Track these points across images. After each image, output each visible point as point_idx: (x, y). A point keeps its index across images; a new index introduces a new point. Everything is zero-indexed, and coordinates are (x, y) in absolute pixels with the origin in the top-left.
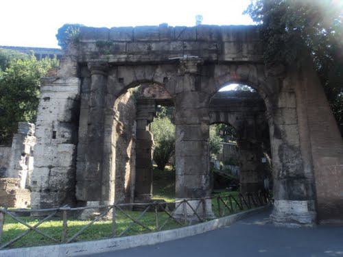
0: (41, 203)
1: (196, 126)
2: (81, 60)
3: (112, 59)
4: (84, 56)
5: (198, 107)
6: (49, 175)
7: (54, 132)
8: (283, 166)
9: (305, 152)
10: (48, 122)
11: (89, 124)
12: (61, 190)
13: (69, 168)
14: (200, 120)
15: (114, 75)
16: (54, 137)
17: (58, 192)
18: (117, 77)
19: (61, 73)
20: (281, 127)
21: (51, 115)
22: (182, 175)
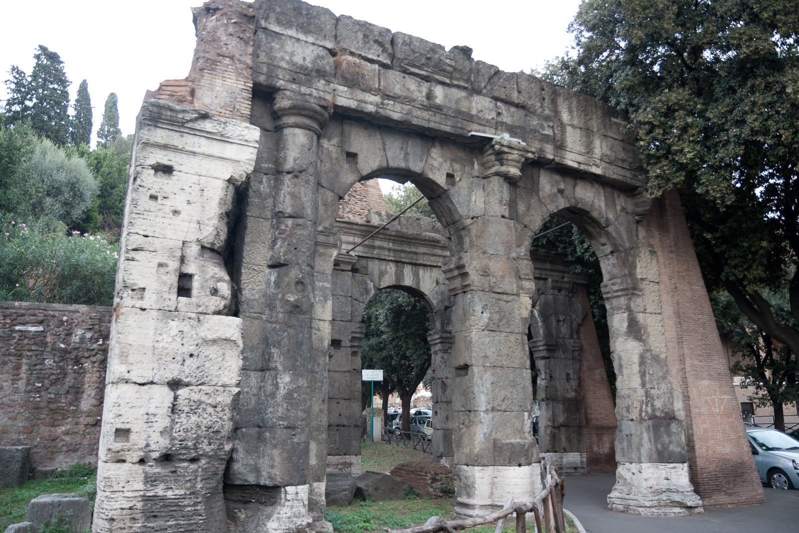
0: (146, 499)
2: (262, 79)
3: (345, 98)
4: (272, 67)
5: (514, 255)
6: (174, 409)
8: (647, 396)
9: (674, 369)
10: (171, 244)
14: (518, 287)
15: (335, 141)
16: (184, 290)
17: (203, 461)
19: (206, 99)
20: (640, 317)
21: (177, 220)
22: (486, 411)
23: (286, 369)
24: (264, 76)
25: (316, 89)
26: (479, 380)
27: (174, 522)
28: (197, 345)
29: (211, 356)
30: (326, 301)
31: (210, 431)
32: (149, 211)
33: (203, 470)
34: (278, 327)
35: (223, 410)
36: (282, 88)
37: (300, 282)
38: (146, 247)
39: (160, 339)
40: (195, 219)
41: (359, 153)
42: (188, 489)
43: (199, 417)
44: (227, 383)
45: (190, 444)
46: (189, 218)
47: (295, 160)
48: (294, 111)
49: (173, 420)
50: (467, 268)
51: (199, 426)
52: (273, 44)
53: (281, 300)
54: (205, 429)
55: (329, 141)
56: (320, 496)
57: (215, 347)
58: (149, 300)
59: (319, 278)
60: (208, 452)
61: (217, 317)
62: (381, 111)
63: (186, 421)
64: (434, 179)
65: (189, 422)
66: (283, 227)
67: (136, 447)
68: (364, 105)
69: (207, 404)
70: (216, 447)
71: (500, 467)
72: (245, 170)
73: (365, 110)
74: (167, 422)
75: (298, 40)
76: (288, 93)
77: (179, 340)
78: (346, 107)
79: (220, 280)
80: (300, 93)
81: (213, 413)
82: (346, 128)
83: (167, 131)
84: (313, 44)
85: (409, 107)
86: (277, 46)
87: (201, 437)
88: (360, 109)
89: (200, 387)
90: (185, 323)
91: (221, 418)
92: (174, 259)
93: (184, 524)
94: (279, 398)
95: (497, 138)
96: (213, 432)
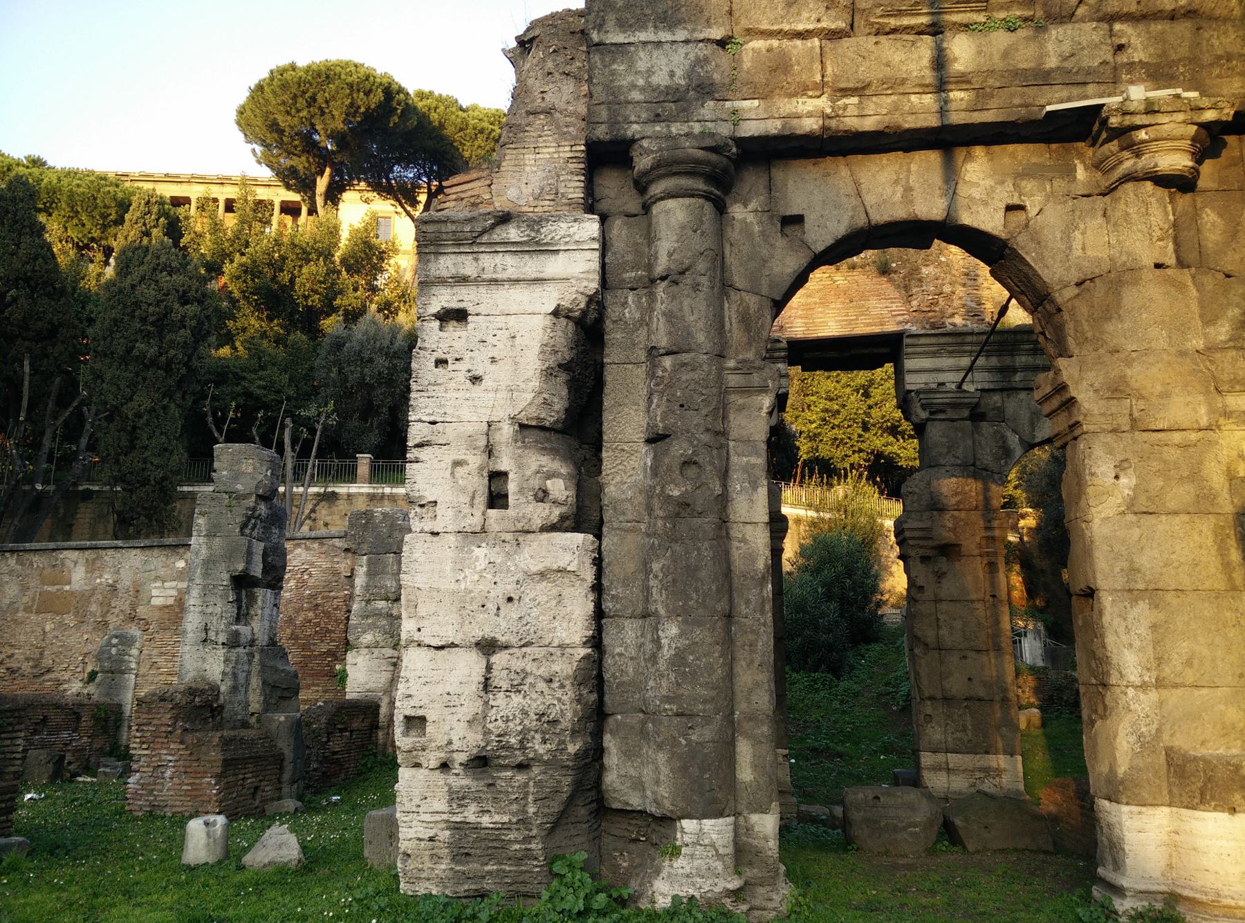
0: (456, 827)
1: (1193, 436)
2: (601, 132)
4: (616, 102)
6: (487, 685)
7: (497, 477)
10: (469, 429)
11: (655, 439)
12: (551, 764)
13: (583, 652)
14: (1211, 411)
16: (497, 499)
17: (536, 770)
18: (768, 211)
21: (477, 390)
23: (673, 613)
24: (604, 126)
25: (699, 121)
26: (1117, 621)
27: (495, 867)
28: (518, 582)
29: (539, 599)
30: (755, 488)
31: (543, 719)
32: (436, 384)
33: (538, 784)
34: (656, 542)
35: (562, 686)
36: (637, 136)
37: (687, 463)
38: (434, 439)
39: (461, 578)
40: (503, 385)
41: (805, 213)
42: (513, 814)
43: (524, 697)
44: (567, 642)
45: (513, 741)
46: (494, 385)
47: (670, 255)
48: (662, 171)
49: (486, 703)
50: (1071, 389)
51: (525, 713)
52: (615, 66)
53: (659, 495)
54: (535, 717)
55: (745, 206)
56: (766, 839)
57: (544, 583)
58: (444, 519)
59: (739, 450)
60: (542, 755)
61: (545, 536)
62: (833, 124)
63: (505, 705)
64: (975, 225)
65: (511, 706)
66: (660, 373)
67: (433, 745)
68: (795, 122)
69: (536, 677)
70: (554, 747)
71: (1183, 811)
72: (581, 290)
73: (798, 132)
74: (477, 707)
75: (659, 44)
76: (645, 143)
77: (489, 576)
78: (759, 137)
79: (551, 475)
80: (669, 137)
81: (546, 691)
82: (778, 174)
83: (453, 256)
84: (687, 42)
85: (894, 98)
86: (622, 68)
87: (530, 730)
88: (787, 133)
89: (524, 650)
90: (497, 548)
91: (559, 700)
92: (475, 452)
93: (510, 871)
94: (662, 665)
95: (1113, 101)
96: (548, 721)
